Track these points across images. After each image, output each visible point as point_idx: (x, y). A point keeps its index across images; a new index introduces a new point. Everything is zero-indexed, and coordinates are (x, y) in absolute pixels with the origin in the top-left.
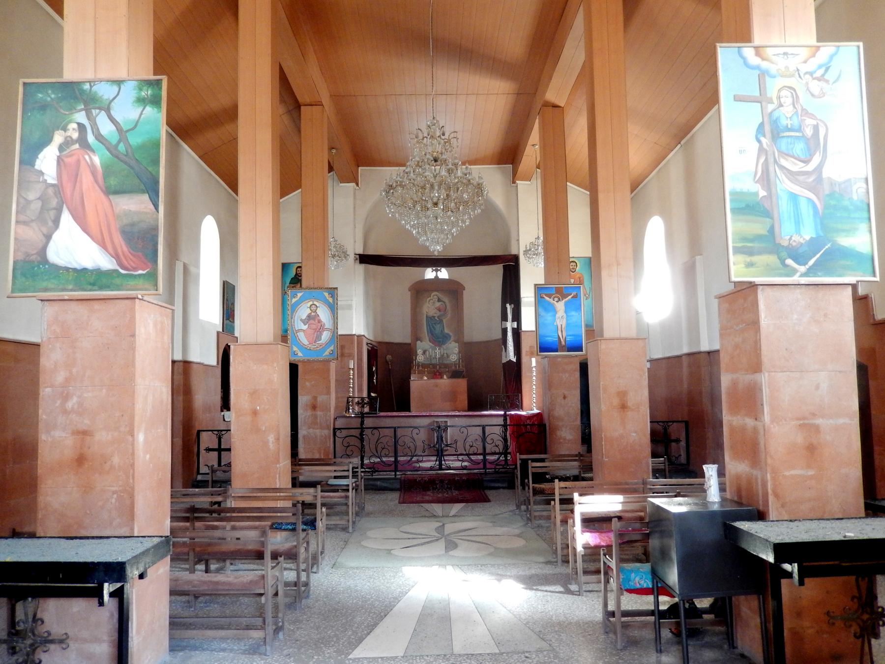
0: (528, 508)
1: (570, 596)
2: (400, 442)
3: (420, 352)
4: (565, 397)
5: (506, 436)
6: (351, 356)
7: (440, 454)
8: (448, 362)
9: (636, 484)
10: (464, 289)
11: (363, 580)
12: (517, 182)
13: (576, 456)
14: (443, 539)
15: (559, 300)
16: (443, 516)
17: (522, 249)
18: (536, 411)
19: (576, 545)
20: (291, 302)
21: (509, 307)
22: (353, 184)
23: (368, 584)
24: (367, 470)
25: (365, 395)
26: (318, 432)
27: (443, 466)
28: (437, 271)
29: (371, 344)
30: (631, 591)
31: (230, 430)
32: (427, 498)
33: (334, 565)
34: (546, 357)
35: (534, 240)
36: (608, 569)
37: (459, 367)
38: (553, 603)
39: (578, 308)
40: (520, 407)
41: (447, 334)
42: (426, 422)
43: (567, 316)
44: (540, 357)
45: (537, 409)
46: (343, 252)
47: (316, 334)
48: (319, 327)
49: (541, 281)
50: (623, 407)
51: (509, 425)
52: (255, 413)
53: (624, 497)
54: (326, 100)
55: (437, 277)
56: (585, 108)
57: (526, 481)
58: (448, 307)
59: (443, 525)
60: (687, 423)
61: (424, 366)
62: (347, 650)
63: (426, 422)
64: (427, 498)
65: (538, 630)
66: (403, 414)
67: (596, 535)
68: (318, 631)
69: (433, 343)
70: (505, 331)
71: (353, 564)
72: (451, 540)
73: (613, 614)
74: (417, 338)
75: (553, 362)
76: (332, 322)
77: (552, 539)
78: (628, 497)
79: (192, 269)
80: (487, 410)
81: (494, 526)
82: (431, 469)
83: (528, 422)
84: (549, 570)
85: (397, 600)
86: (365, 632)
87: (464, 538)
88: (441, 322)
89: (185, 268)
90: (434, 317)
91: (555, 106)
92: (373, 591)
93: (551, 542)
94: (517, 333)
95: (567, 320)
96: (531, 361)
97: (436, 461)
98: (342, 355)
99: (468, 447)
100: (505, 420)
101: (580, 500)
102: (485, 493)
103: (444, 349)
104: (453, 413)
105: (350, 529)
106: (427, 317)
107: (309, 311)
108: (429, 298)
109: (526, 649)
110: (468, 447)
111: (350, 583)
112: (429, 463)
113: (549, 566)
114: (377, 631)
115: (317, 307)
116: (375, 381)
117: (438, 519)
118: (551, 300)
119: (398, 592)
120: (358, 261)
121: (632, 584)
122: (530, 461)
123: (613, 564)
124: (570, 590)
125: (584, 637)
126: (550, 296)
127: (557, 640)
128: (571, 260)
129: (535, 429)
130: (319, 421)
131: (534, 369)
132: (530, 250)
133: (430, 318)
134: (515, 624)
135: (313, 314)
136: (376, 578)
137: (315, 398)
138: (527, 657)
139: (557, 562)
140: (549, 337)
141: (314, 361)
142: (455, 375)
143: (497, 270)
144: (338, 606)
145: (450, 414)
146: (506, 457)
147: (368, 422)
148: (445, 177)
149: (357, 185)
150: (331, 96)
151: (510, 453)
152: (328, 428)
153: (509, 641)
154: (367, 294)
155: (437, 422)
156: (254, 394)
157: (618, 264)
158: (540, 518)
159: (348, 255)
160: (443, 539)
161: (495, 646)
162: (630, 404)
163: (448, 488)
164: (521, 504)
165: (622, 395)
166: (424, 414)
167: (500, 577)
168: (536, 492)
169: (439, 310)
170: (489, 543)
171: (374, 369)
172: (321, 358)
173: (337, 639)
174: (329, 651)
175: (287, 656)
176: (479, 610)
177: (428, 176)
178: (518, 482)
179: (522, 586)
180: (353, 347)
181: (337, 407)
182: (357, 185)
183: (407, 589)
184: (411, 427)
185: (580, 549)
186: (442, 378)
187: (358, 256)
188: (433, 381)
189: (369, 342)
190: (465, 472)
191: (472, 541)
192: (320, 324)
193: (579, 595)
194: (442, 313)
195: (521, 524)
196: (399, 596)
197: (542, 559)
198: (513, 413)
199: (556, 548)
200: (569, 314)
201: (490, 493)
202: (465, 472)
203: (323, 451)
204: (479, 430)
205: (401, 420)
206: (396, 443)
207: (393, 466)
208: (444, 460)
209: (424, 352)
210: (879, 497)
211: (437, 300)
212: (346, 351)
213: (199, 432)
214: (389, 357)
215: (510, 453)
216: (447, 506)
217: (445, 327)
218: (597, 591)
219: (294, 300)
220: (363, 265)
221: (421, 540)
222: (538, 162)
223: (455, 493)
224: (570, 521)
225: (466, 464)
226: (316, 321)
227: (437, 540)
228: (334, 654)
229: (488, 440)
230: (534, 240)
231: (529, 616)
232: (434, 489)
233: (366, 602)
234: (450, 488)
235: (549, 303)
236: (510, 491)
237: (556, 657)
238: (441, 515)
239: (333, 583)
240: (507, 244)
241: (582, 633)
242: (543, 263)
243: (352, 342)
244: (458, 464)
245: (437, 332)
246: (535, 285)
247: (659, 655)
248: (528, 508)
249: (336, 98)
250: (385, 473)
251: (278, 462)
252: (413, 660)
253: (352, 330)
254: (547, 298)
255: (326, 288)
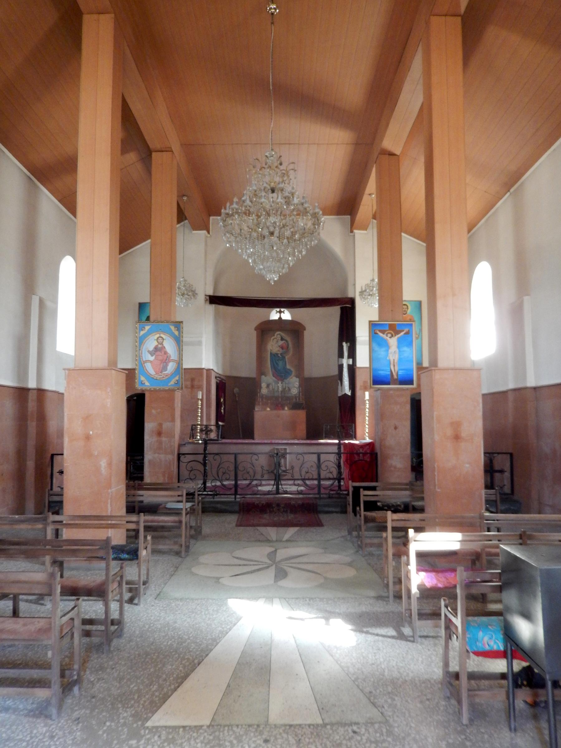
0: (359, 534)
1: (403, 643)
2: (241, 468)
3: (264, 385)
4: (396, 428)
5: (339, 463)
6: (200, 388)
7: (278, 479)
8: (290, 395)
9: (473, 517)
10: (305, 329)
11: (184, 615)
12: (355, 231)
13: (407, 484)
14: (274, 566)
15: (392, 336)
16: (277, 541)
17: (358, 290)
18: (368, 440)
19: (410, 585)
20: (139, 334)
21: (345, 346)
22: (204, 232)
23: (189, 620)
24: (209, 493)
25: (213, 422)
26: (162, 456)
27: (280, 491)
28: (280, 312)
29: (220, 378)
30: (477, 654)
31: (62, 454)
32: (264, 521)
33: (159, 594)
34: (379, 389)
35: (369, 282)
36: (449, 625)
37: (299, 399)
38: (385, 651)
39: (410, 344)
40: (354, 437)
41: (290, 370)
42: (267, 449)
43: (400, 351)
44: (373, 389)
45: (370, 438)
46: (192, 291)
47: (162, 364)
48: (165, 358)
49: (375, 317)
50: (457, 437)
51: (343, 453)
52: (88, 438)
53: (463, 535)
54: (176, 147)
55: (280, 318)
56: (422, 159)
57: (358, 508)
58: (291, 345)
59: (276, 550)
60: (511, 455)
61: (268, 398)
62: (146, 714)
63: (267, 449)
64: (264, 521)
65: (367, 690)
66: (247, 441)
67: (433, 575)
68: (120, 683)
69: (276, 378)
70: (341, 367)
71: (178, 595)
72: (281, 568)
73: (457, 676)
74: (261, 372)
75: (385, 395)
76: (177, 353)
77: (383, 569)
78: (472, 536)
79: (48, 304)
80: (322, 439)
81: (325, 553)
82: (269, 493)
83: (361, 450)
84: (379, 607)
85: (215, 641)
86: (173, 687)
87: (294, 565)
88: (284, 358)
89: (41, 301)
90: (277, 354)
91: (392, 154)
92: (191, 630)
93: (381, 572)
94: (352, 369)
95: (400, 355)
96: (364, 394)
97: (274, 485)
98: (192, 387)
99: (303, 473)
100: (339, 448)
101: (415, 537)
102: (319, 518)
103: (286, 383)
104: (292, 441)
105: (183, 554)
106: (271, 353)
107: (155, 343)
108: (273, 338)
109: (355, 719)
110: (303, 473)
111: (170, 618)
112: (267, 487)
113: (380, 601)
114: (187, 684)
115: (163, 339)
116: (222, 411)
117: (271, 544)
118: (384, 336)
119: (217, 632)
120: (208, 302)
121: (480, 644)
122: (361, 490)
123: (457, 621)
124: (403, 634)
125: (421, 702)
126: (383, 332)
127: (390, 706)
128: (404, 303)
129: (367, 458)
130: (163, 446)
131: (367, 402)
132: (365, 291)
133: (274, 355)
134: (342, 681)
135: (160, 346)
136: (199, 612)
137: (160, 425)
138: (354, 732)
139: (388, 597)
140: (383, 370)
141: (160, 390)
142: (296, 406)
143: (335, 312)
144: (151, 649)
145: (289, 442)
146: (339, 482)
147: (211, 448)
148: (282, 204)
149: (209, 232)
150: (181, 144)
151: (343, 479)
152: (172, 453)
153: (334, 705)
154: (217, 333)
155: (277, 449)
156: (87, 419)
157: (454, 295)
158: (371, 545)
159: (196, 294)
160: (274, 566)
161: (318, 712)
162: (463, 435)
163: (284, 511)
164: (353, 531)
165: (456, 425)
166: (266, 442)
167: (328, 615)
168: (367, 520)
169: (282, 347)
170: (319, 572)
171: (222, 400)
172: (167, 388)
173: (138, 697)
174: (126, 714)
175: (75, 720)
176: (303, 658)
177: (264, 202)
178: (350, 508)
179: (350, 627)
180: (202, 380)
181: (182, 433)
182: (209, 232)
183: (228, 627)
184: (251, 453)
185: (414, 590)
186: (283, 409)
187: (208, 298)
188: (275, 412)
189: (218, 375)
190: (301, 496)
191: (304, 570)
192: (165, 356)
193: (413, 642)
194: (284, 350)
195: (352, 552)
196: (218, 636)
197: (372, 593)
198: (347, 442)
199: (388, 582)
200: (402, 350)
201: (323, 518)
202: (301, 496)
203: (167, 475)
204: (315, 457)
205: (240, 446)
206: (236, 468)
207: (233, 489)
208: (281, 485)
209: (268, 386)
210: (125, 375)
211: (280, 339)
212: (196, 383)
213: (53, 455)
214: (236, 390)
215: (343, 479)
216: (281, 529)
217: (287, 363)
218: (433, 637)
219: (142, 333)
220: (214, 305)
221: (252, 566)
222: (374, 212)
223: (291, 516)
224: (404, 558)
225: (302, 488)
226: (163, 353)
227: (268, 567)
228: (131, 719)
229: (323, 466)
230: (369, 282)
231: (358, 670)
232: (271, 512)
233: (182, 644)
234: (286, 512)
235: (383, 338)
236: (343, 515)
237: (390, 733)
238: (274, 539)
239: (152, 618)
240: (344, 286)
241: (419, 696)
242: (377, 303)
243: (202, 375)
244: (294, 488)
245: (279, 368)
246: (370, 322)
247: (513, 735)
248: (359, 534)
249: (187, 146)
250: (226, 496)
251: (110, 487)
252: (220, 731)
253: (201, 364)
254: (381, 334)
255: (173, 322)
